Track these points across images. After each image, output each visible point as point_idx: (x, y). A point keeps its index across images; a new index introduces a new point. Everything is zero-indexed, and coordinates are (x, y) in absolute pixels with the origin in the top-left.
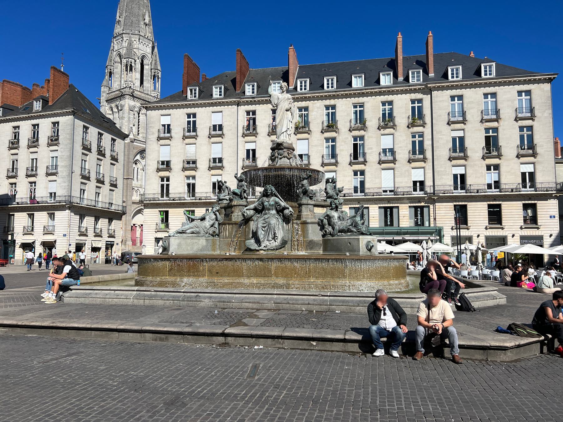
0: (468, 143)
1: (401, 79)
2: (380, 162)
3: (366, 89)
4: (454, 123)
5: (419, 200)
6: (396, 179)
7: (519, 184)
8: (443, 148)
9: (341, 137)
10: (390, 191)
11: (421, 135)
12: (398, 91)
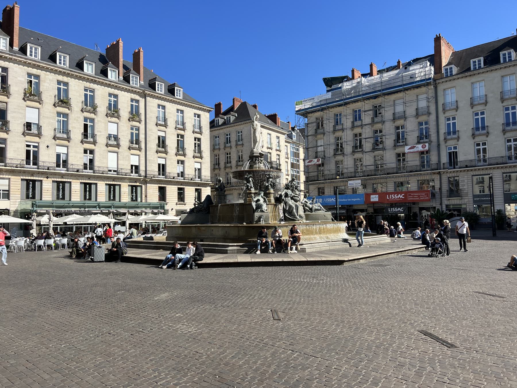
0: (167, 142)
1: (16, 48)
2: (107, 145)
3: (9, 54)
5: (136, 180)
6: (119, 162)
7: (23, 160)
8: (153, 144)
9: (73, 115)
10: (114, 171)
11: (138, 129)
12: (123, 88)
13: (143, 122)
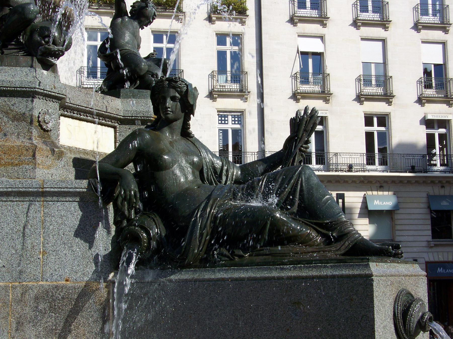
11: (237, 39)
13: (251, 20)
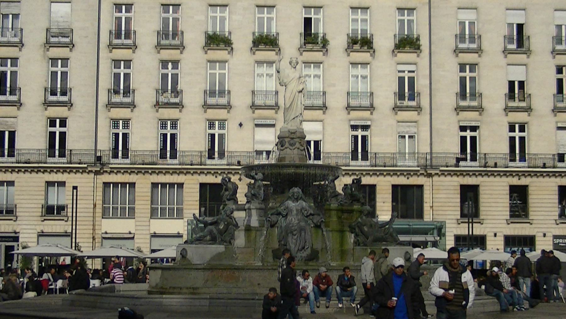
4: (463, 51)
8: (447, 95)
